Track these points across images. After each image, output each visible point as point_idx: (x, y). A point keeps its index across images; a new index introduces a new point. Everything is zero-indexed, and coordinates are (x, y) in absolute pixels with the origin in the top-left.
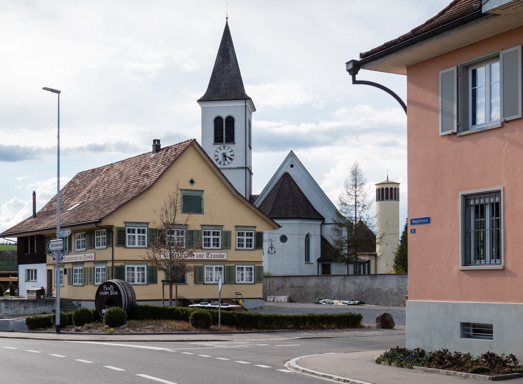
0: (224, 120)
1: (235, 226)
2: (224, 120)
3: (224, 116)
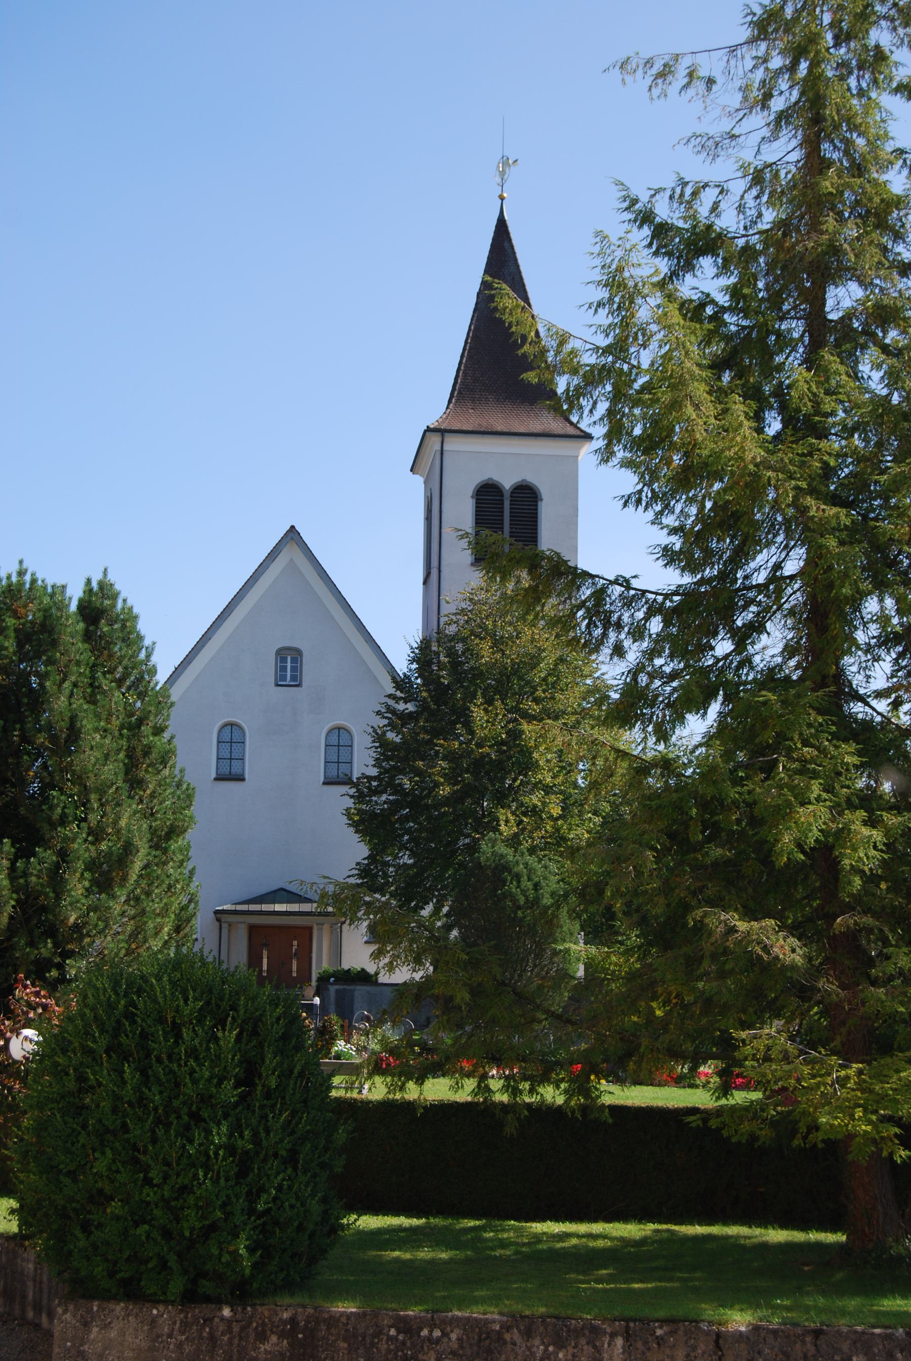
0: (507, 496)
1: (293, 527)
2: (507, 496)
3: (507, 483)
